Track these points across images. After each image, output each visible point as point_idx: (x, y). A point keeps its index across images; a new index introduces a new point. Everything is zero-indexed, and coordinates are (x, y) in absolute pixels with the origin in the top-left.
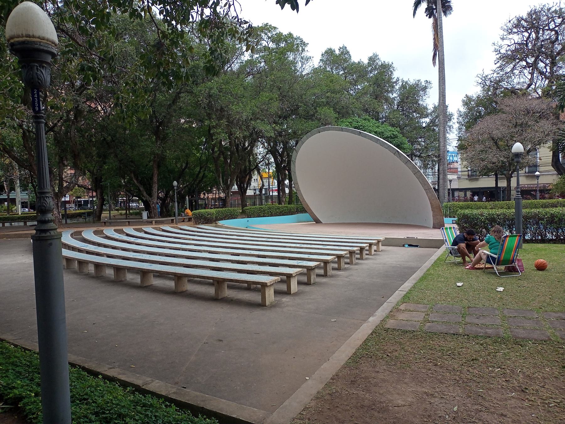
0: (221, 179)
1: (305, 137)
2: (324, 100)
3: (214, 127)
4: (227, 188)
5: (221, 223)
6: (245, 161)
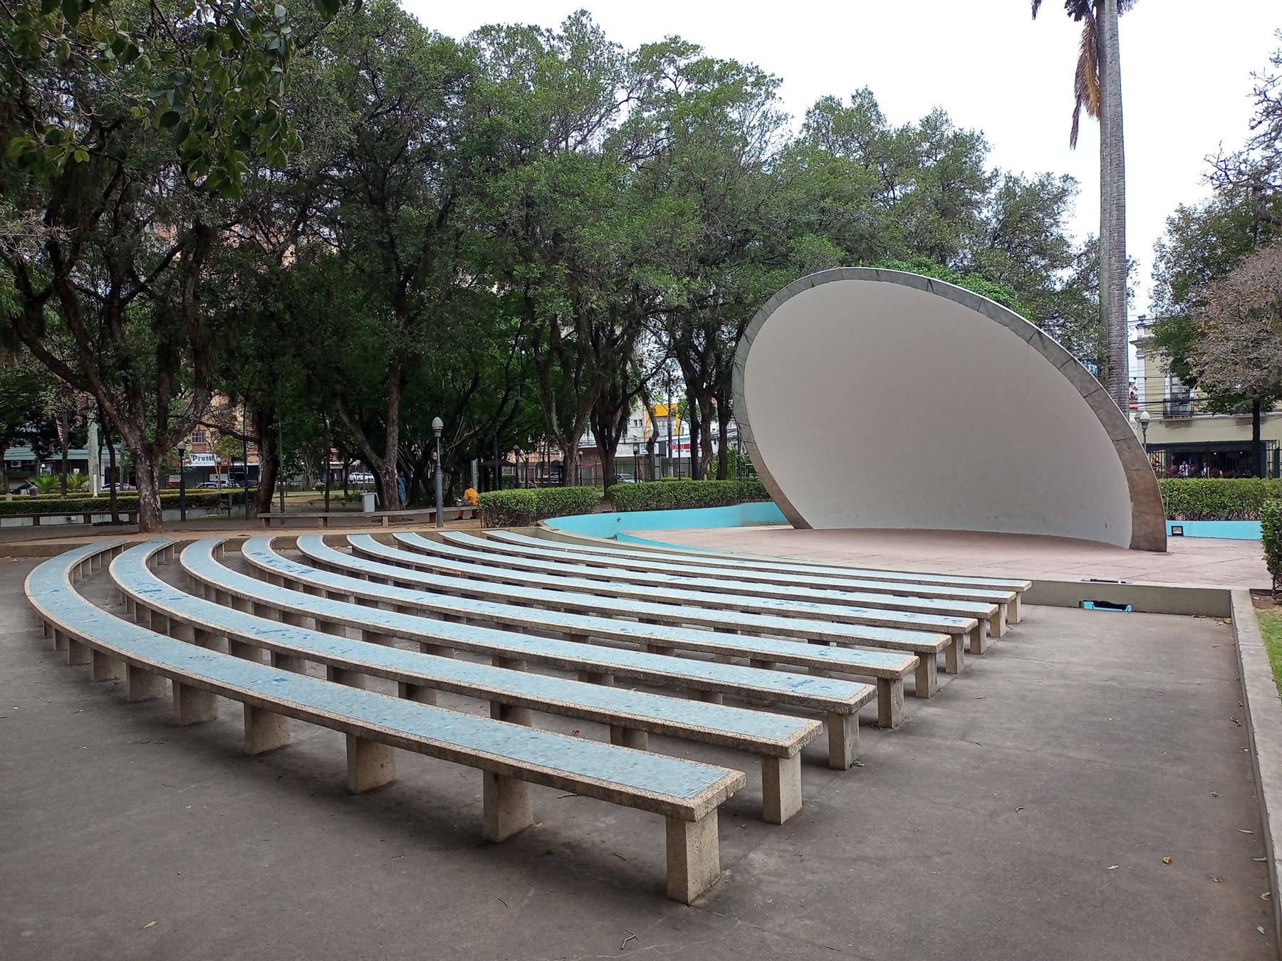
0: (554, 417)
1: (765, 307)
2: (813, 217)
3: (538, 282)
4: (570, 436)
5: (550, 524)
6: (614, 371)
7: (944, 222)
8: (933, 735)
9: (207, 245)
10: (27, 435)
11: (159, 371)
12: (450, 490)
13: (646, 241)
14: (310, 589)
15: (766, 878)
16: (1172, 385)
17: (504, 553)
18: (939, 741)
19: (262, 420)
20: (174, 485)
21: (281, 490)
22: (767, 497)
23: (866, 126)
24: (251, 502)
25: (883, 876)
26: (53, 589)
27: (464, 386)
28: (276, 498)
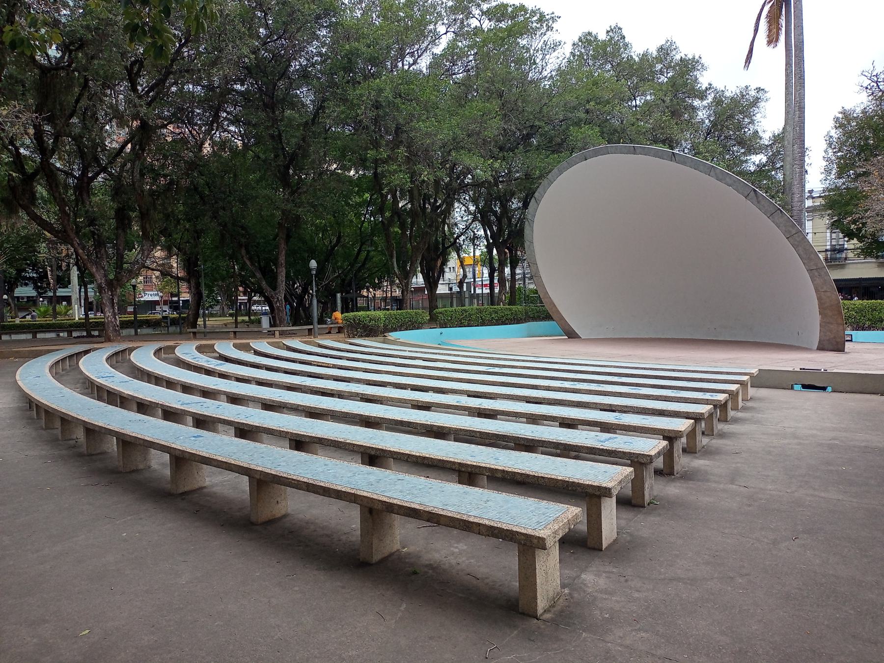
0: (395, 260)
3: (385, 162)
4: (406, 276)
5: (393, 335)
6: (437, 229)
7: (673, 122)
8: (708, 480)
9: (149, 138)
10: (30, 278)
11: (117, 228)
12: (322, 314)
13: (461, 134)
14: (223, 376)
15: (600, 595)
16: (831, 239)
17: (362, 353)
18: (714, 485)
19: (190, 264)
20: (130, 313)
21: (204, 315)
22: (548, 317)
23: (616, 52)
24: (184, 322)
25: (697, 594)
26: (37, 378)
27: (331, 242)
28: (200, 321)
